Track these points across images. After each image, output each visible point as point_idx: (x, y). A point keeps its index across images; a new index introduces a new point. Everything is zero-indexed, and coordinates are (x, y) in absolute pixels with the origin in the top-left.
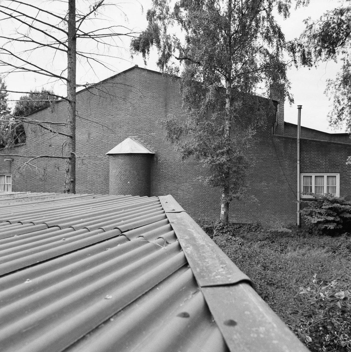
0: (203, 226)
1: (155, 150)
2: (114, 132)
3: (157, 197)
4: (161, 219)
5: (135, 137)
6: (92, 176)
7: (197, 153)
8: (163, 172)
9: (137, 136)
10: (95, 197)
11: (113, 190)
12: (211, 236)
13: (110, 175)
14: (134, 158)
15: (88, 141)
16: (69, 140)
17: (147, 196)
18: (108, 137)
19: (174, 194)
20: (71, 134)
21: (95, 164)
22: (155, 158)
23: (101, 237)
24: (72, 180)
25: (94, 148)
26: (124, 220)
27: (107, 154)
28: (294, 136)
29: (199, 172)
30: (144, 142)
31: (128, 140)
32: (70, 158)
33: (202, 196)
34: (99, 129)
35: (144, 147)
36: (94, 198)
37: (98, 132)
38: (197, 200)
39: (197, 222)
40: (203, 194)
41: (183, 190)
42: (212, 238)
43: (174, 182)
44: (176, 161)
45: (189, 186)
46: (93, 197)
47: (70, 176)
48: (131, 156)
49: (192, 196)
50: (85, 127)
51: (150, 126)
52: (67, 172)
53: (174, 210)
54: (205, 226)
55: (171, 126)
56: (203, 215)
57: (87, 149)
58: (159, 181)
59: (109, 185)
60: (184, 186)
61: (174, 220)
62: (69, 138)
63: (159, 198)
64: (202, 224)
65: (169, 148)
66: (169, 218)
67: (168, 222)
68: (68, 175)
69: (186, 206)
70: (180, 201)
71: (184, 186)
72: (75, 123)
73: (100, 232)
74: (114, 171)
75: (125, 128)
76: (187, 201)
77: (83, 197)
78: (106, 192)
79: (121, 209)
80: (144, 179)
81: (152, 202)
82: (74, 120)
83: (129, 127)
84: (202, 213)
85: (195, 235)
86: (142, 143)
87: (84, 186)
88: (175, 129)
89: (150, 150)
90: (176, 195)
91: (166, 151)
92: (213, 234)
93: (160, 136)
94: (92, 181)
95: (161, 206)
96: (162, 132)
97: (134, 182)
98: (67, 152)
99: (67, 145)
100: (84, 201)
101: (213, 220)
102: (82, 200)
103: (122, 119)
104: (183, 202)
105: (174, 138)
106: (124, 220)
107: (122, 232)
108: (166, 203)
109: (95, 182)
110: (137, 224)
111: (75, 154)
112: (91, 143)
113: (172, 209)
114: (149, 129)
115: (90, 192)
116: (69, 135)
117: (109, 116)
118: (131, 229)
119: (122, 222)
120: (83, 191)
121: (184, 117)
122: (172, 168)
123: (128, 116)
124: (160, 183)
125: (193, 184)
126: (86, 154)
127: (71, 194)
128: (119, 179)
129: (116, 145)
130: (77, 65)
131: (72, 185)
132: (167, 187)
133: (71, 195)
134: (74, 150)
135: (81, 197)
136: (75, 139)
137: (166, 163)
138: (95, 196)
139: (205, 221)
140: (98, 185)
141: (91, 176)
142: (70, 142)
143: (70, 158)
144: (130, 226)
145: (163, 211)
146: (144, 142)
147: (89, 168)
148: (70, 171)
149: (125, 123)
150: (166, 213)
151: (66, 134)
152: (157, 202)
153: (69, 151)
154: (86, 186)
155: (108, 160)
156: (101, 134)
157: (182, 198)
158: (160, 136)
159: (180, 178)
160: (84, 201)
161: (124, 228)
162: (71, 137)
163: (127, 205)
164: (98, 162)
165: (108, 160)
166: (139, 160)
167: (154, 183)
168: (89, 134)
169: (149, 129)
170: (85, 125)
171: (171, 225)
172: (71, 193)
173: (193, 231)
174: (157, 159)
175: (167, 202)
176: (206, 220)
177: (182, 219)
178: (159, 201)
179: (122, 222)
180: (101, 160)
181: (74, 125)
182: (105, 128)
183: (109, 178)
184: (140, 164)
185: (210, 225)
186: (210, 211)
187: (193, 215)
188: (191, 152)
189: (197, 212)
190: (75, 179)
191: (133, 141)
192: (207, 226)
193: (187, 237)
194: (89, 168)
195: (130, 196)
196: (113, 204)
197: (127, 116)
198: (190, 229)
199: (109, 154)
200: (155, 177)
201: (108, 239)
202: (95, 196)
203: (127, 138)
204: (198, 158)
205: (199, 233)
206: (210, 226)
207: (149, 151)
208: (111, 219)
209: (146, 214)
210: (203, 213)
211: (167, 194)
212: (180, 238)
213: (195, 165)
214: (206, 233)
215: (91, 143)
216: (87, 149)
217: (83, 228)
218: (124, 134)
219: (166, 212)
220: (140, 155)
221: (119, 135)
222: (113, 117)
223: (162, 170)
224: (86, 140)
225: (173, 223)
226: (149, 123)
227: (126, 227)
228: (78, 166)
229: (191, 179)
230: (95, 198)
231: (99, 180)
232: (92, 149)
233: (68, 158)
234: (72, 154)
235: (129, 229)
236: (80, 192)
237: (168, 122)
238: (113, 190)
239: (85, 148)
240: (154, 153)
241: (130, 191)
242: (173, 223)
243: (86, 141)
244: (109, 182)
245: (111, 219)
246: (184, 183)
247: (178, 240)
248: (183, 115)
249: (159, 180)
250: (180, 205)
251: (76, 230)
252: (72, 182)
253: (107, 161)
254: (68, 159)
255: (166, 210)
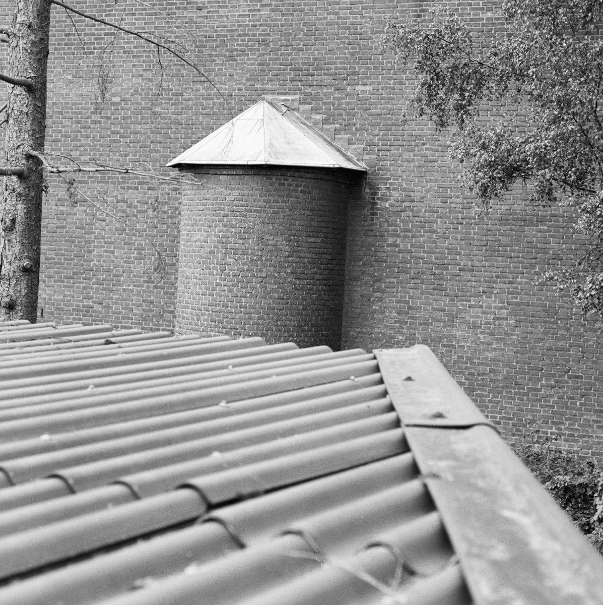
0: (550, 478)
1: (367, 157)
2: (204, 77)
3: (369, 351)
4: (382, 452)
5: (290, 98)
6: (113, 252)
7: (544, 176)
8: (396, 246)
9: (297, 97)
10: (113, 339)
11: (189, 310)
12: (584, 520)
13: (182, 247)
14: (279, 184)
15: (98, 109)
16: (20, 101)
17: (325, 347)
18: (181, 94)
19: (439, 340)
20: (28, 75)
21: (125, 201)
22: (367, 190)
23: (118, 523)
24: (26, 263)
25: (121, 137)
26: (224, 447)
27: (174, 166)
28: (92, 324)
29: (546, 253)
30: (326, 121)
31: (258, 111)
32: (20, 175)
33: (550, 353)
34: (144, 62)
35: (321, 140)
36: (108, 343)
37: (141, 76)
38: (530, 369)
39: (527, 462)
40: (559, 344)
41: (475, 326)
42: (587, 529)
43: (439, 289)
44: (453, 205)
45: (501, 308)
46: (103, 341)
47: (17, 248)
48: (269, 177)
49: (509, 352)
50: (92, 53)
51: (353, 54)
52: (9, 229)
53: (440, 416)
54: (561, 477)
55: (437, 55)
56: (552, 433)
57: (94, 139)
58: (377, 285)
59: (176, 288)
60: (481, 307)
61: (443, 464)
62: (19, 90)
63: (375, 358)
64: (547, 471)
65: (427, 149)
66: (418, 452)
67: (414, 471)
68: (9, 241)
69: (483, 390)
70: (459, 368)
71: (481, 307)
72: (46, 33)
73: (117, 501)
74: (198, 236)
75: (250, 62)
76: (488, 369)
77: (65, 338)
78: (162, 316)
79: (213, 400)
80: (316, 273)
81: (345, 376)
82: (42, 21)
83: (267, 57)
84: (547, 423)
85: (537, 542)
86: (315, 123)
87: (78, 287)
88: (455, 67)
89: (349, 154)
90: (445, 346)
91: (413, 160)
92: (593, 515)
93: (393, 99)
94: (108, 271)
95: (381, 381)
96: (401, 83)
97: (276, 283)
98: (13, 148)
99: (11, 121)
100: (66, 355)
101: (593, 454)
102: (59, 349)
103: (239, 26)
104: (472, 374)
105: (451, 105)
106: (224, 447)
107: (211, 507)
108: (409, 383)
109: (121, 276)
110: (281, 472)
111: (42, 158)
112: (113, 117)
113: (435, 410)
114: (345, 69)
115: (101, 312)
116: (16, 78)
117: (186, 9)
118: (254, 495)
119: (216, 456)
120: (71, 308)
121: (493, 24)
122: (434, 232)
123: (265, 12)
124: (383, 291)
125: (519, 304)
126: (90, 160)
127: (18, 321)
128: (214, 268)
129: (213, 129)
130: (306, 165)
131: (23, 284)
132: (410, 308)
133: (18, 324)
134: (39, 141)
135: (54, 336)
136: (43, 99)
137: (412, 211)
138: (114, 336)
139: (560, 458)
140: (131, 287)
141: (105, 251)
142: (25, 110)
143: (20, 175)
144: (248, 480)
145: (391, 416)
146: (326, 121)
147: (99, 220)
148: (19, 227)
149: (249, 40)
150: (408, 426)
151: (10, 76)
152: (366, 374)
153: (18, 147)
154: (85, 288)
155: (176, 189)
156: (151, 80)
157: (470, 359)
158: (393, 99)
159: (467, 276)
160: (66, 355)
161: (221, 487)
162: (29, 88)
163: (243, 381)
164: (135, 196)
165: (176, 189)
166: (301, 194)
167: (358, 290)
168: (104, 82)
169: (345, 69)
170: (92, 43)
171: (425, 486)
172: (21, 318)
173: (525, 521)
174: (376, 194)
175: (409, 379)
176: (564, 454)
177: (475, 462)
178: (377, 369)
179: (216, 456)
180: (150, 189)
181: (42, 39)
182: (166, 58)
183: (177, 260)
184: (307, 212)
185: (580, 474)
186: (582, 415)
187: (511, 430)
188: (517, 169)
189: (530, 417)
190: (36, 262)
191: (279, 115)
192: (567, 478)
193: (500, 553)
194: (99, 220)
195: (258, 344)
196: (182, 374)
197: (259, 10)
198: (513, 510)
199: (180, 167)
200: (364, 265)
201: (147, 536)
202: (114, 336)
203: (254, 101)
204: (550, 193)
205: (554, 536)
206: (581, 480)
207: (342, 158)
208: (169, 442)
209: (317, 425)
210: (553, 423)
211: (411, 341)
212: (470, 555)
213: (531, 224)
214: (564, 508)
215: (113, 117)
216: (94, 139)
217: (47, 474)
218: (245, 84)
219: (405, 421)
220: (307, 175)
221: (225, 89)
222: (204, 13)
223: (390, 240)
224: (92, 103)
225: (435, 476)
226: (350, 44)
227: (231, 484)
228: (49, 208)
229: (510, 283)
230: (111, 343)
231: (136, 268)
232: (114, 141)
233: (14, 173)
234: (29, 157)
235: (246, 490)
236: (59, 315)
237: (427, 36)
238: (189, 310)
239: (88, 137)
240: (362, 166)
241: (259, 318)
242: (435, 476)
243: (93, 106)
244: (176, 279)
245: (169, 442)
246: (478, 295)
247: (458, 562)
248: (489, 14)
249: (380, 281)
250: (461, 384)
251: (14, 480)
252: (25, 270)
253: (173, 194)
254: (14, 178)
255: (407, 412)
